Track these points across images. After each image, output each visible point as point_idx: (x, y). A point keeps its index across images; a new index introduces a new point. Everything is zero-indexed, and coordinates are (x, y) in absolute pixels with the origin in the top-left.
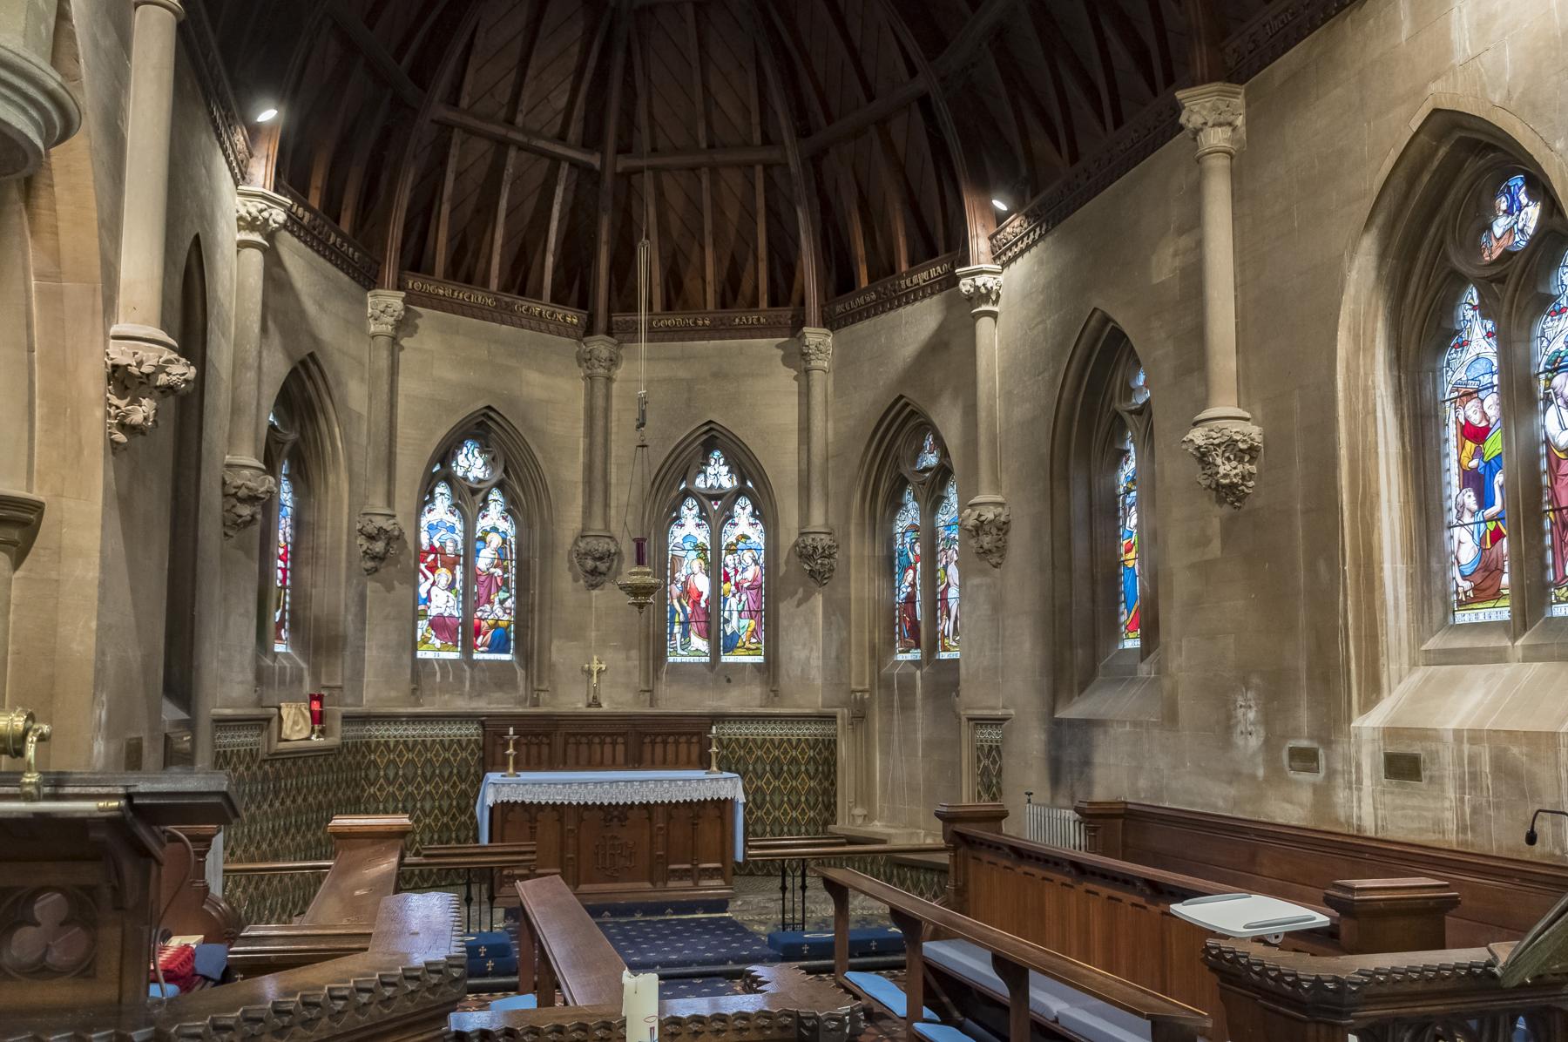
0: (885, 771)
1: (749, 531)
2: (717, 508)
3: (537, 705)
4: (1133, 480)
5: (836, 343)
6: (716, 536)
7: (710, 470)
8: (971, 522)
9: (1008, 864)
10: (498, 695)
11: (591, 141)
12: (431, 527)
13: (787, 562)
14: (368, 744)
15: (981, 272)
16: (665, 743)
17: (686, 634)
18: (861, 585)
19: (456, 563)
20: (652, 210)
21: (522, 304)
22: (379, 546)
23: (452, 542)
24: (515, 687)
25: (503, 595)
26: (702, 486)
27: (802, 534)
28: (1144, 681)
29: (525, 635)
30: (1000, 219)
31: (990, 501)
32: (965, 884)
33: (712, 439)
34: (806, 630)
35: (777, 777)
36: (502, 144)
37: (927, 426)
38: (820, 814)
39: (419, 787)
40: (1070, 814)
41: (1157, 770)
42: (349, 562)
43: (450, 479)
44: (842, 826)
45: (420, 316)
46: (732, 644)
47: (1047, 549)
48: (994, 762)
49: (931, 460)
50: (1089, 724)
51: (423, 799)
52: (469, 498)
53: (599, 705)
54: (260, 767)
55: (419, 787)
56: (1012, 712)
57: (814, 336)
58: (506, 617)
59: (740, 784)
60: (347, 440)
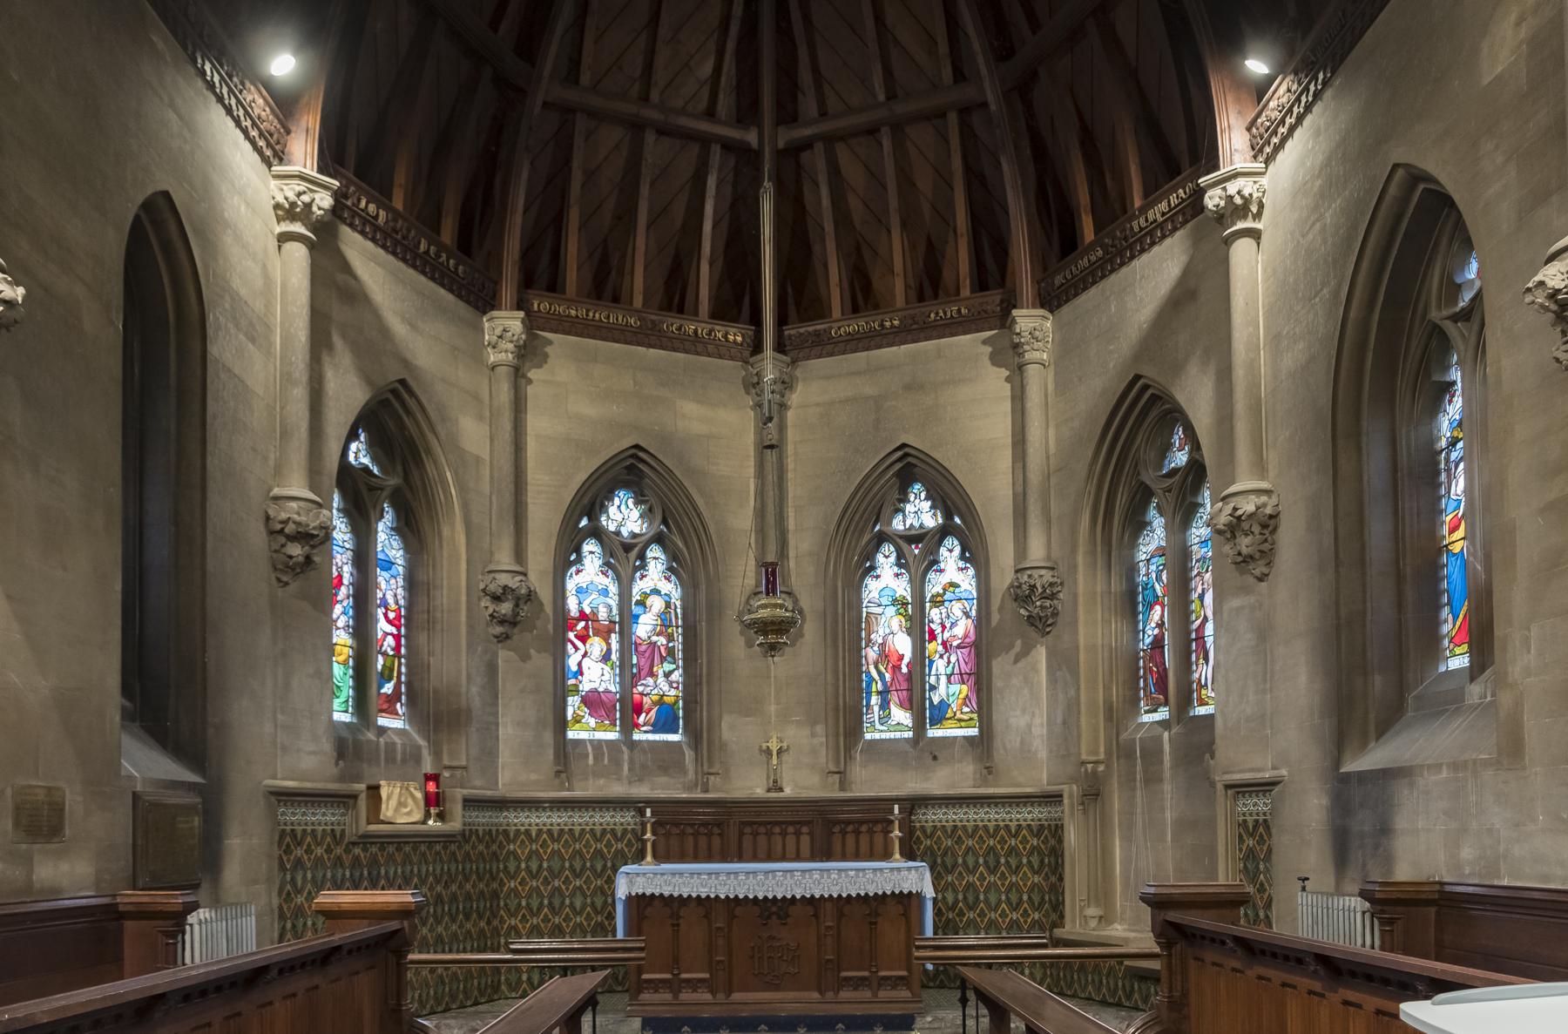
0: (1126, 862)
1: (957, 577)
2: (919, 552)
3: (706, 791)
4: (1460, 424)
5: (1058, 327)
6: (918, 585)
7: (909, 508)
8: (1224, 519)
9: (1237, 965)
10: (663, 780)
11: (747, 113)
12: (579, 590)
13: (1001, 609)
14: (506, 833)
15: (1236, 175)
16: (871, 832)
17: (885, 705)
18: (1091, 628)
19: (610, 631)
20: (825, 192)
21: (672, 324)
22: (506, 608)
23: (605, 606)
24: (684, 771)
25: (668, 667)
26: (901, 527)
27: (1017, 571)
28: (1474, 708)
29: (695, 712)
30: (1260, 90)
31: (1246, 487)
32: (1185, 995)
33: (908, 469)
34: (1026, 691)
35: (992, 871)
36: (637, 127)
37: (1174, 415)
38: (1047, 915)
39: (567, 881)
40: (1358, 904)
41: (1490, 831)
42: (471, 627)
43: (597, 533)
44: (1070, 930)
45: (550, 343)
46: (940, 714)
47: (1328, 541)
48: (1261, 841)
49: (1180, 458)
50: (1387, 775)
51: (572, 896)
52: (624, 557)
53: (781, 790)
54: (347, 851)
55: (567, 881)
56: (1284, 772)
57: (1028, 320)
58: (673, 692)
59: (928, 875)
60: (462, 489)
